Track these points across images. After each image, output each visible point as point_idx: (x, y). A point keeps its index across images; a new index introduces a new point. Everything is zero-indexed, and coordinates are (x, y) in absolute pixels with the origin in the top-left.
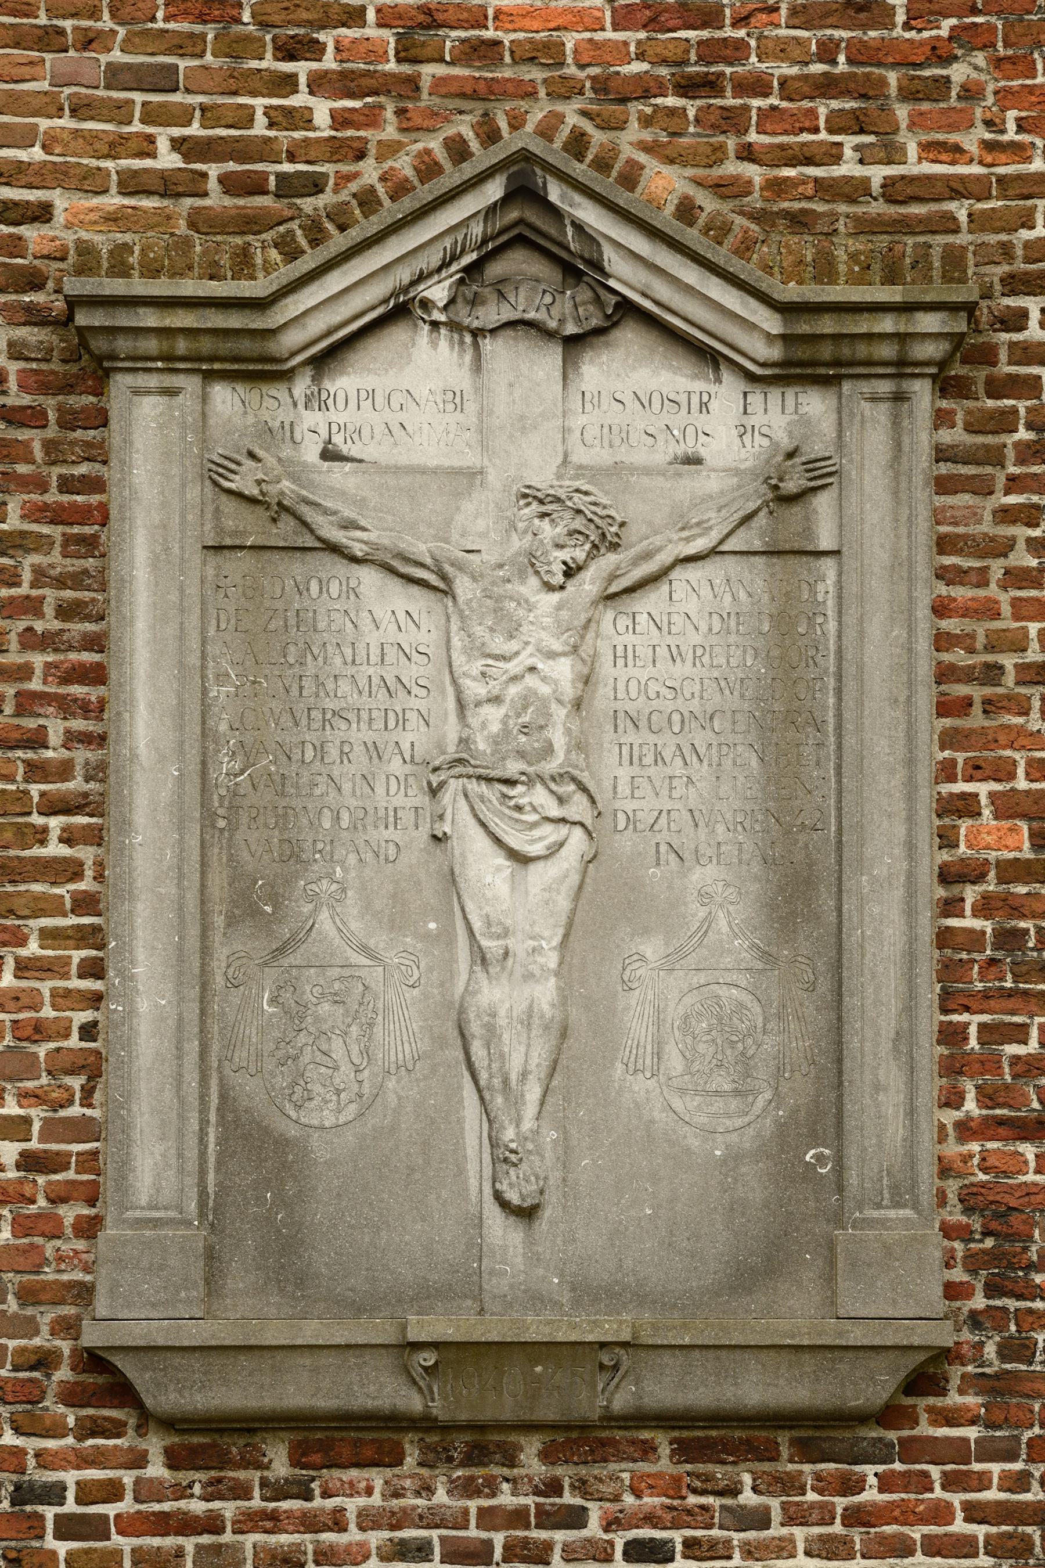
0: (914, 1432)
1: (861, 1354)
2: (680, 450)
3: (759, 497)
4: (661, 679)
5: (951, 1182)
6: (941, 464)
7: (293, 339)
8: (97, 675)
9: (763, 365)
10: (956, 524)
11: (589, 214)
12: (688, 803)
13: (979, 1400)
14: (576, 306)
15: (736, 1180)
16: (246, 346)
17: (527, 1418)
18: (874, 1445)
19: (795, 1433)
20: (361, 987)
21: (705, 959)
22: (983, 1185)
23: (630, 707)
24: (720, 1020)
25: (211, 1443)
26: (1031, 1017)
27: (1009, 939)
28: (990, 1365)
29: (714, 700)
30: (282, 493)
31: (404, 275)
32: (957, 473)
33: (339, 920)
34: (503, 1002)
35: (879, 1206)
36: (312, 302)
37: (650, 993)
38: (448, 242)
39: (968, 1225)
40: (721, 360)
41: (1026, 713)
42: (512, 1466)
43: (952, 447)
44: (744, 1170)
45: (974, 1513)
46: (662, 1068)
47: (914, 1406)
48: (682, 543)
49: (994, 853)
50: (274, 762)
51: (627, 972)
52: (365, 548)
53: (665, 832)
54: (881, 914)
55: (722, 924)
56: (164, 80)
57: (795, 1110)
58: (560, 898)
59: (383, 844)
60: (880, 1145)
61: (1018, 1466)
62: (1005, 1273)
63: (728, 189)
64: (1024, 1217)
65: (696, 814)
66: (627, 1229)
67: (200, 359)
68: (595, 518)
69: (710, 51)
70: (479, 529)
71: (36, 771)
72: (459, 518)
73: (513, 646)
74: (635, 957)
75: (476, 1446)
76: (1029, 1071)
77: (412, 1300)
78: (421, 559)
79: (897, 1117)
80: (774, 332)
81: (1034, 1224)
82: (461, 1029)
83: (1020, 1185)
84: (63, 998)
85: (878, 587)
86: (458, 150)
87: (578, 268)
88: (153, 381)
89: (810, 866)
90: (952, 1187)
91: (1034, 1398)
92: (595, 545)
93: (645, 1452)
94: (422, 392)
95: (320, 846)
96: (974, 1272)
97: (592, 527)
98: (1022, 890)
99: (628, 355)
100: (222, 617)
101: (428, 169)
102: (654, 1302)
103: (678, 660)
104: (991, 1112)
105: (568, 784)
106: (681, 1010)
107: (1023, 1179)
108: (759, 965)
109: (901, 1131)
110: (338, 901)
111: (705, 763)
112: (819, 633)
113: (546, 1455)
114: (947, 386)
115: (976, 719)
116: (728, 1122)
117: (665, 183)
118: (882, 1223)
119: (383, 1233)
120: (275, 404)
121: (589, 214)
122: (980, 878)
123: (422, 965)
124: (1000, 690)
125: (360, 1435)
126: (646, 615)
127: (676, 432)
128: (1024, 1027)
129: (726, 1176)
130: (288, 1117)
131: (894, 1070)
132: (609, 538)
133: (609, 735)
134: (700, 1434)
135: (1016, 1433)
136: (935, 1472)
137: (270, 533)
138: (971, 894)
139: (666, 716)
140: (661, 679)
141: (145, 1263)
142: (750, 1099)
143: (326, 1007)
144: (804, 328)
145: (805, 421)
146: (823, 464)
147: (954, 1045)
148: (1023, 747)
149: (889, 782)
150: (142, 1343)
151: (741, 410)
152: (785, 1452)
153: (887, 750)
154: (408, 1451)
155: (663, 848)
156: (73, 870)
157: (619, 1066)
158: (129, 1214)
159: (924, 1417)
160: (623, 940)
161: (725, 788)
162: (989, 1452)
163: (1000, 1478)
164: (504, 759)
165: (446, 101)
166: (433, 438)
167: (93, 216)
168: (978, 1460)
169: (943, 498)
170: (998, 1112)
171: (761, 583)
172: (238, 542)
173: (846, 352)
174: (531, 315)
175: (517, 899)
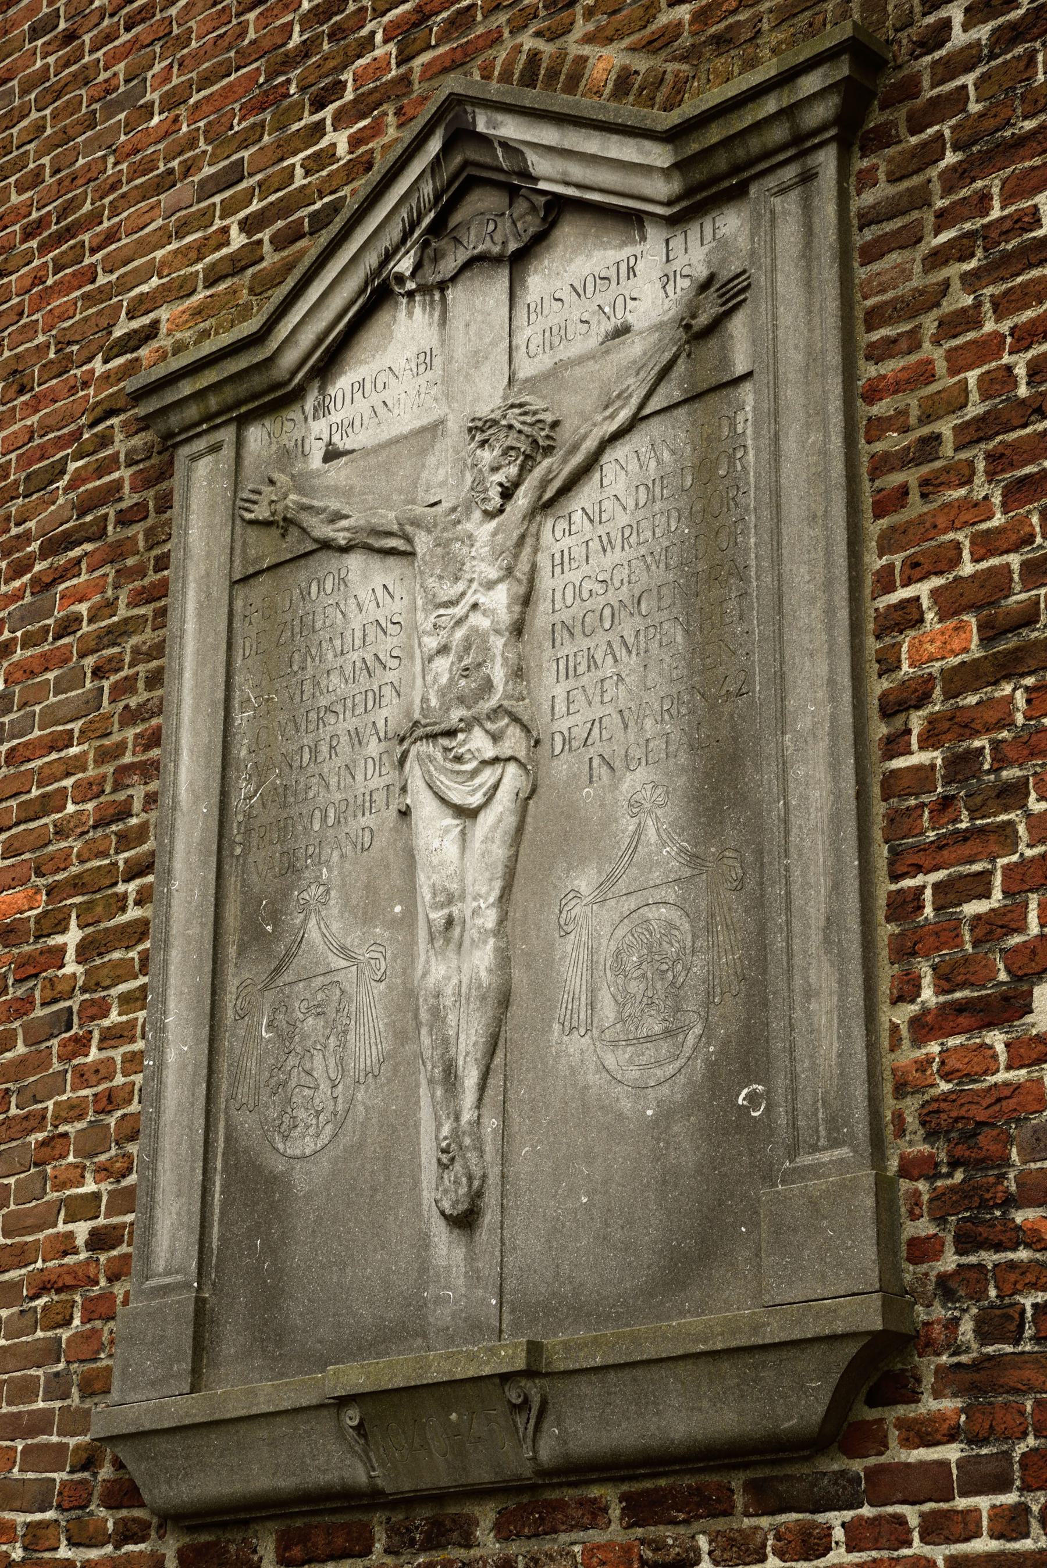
0: (882, 1459)
1: (784, 1354)
2: (609, 326)
3: (675, 344)
4: (593, 576)
5: (909, 1100)
6: (866, 230)
7: (291, 357)
9: (669, 204)
10: (884, 291)
11: (510, 129)
12: (611, 703)
13: (958, 1403)
14: (514, 223)
15: (668, 1143)
16: (257, 382)
17: (463, 1481)
18: (836, 1483)
19: (750, 1474)
20: (338, 992)
21: (635, 880)
22: (945, 1097)
23: (565, 616)
24: (650, 947)
26: (993, 860)
27: (961, 765)
28: (967, 1351)
29: (643, 579)
30: (287, 507)
31: (372, 259)
34: (449, 978)
35: (815, 1149)
36: (297, 319)
37: (584, 932)
38: (404, 213)
39: (931, 1156)
40: (644, 216)
41: (970, 481)
42: (468, 1546)
43: (873, 207)
44: (676, 1129)
46: (596, 1019)
47: (882, 1420)
48: (607, 422)
49: (938, 664)
50: (279, 776)
51: (564, 915)
52: (347, 535)
53: (598, 743)
54: (807, 775)
55: (651, 832)
57: (726, 1042)
58: (494, 846)
59: (360, 832)
60: (814, 1067)
61: (1011, 1498)
62: (978, 1217)
64: (995, 1132)
65: (626, 713)
66: (563, 1226)
67: (229, 409)
68: (525, 428)
72: (424, 475)
73: (460, 587)
74: (571, 896)
76: (991, 932)
77: (371, 1345)
78: (388, 528)
79: (831, 1026)
80: (666, 165)
81: (1010, 1140)
83: (990, 1088)
87: (516, 184)
88: (201, 444)
89: (735, 739)
90: (911, 1106)
91: (1024, 1393)
93: (594, 1516)
94: (400, 364)
95: (311, 850)
96: (940, 1220)
97: (523, 438)
98: (972, 700)
99: (565, 251)
100: (247, 644)
102: (589, 1315)
103: (609, 549)
104: (949, 997)
105: (503, 718)
106: (613, 948)
107: (992, 1079)
108: (687, 872)
109: (836, 1045)
110: (323, 904)
111: (634, 653)
112: (739, 468)
113: (503, 1531)
115: (916, 507)
116: (659, 1072)
118: (814, 1171)
119: (348, 1270)
121: (510, 129)
122: (923, 700)
123: (388, 955)
124: (938, 464)
125: (334, 1519)
126: (580, 512)
127: (607, 309)
128: (986, 876)
129: (658, 1140)
130: (277, 1150)
131: (826, 966)
132: (541, 443)
133: (548, 653)
134: (648, 1485)
135: (1005, 1447)
136: (912, 1514)
138: (917, 722)
139: (598, 614)
140: (593, 576)
141: (149, 1339)
142: (681, 1036)
143: (310, 1021)
144: (694, 147)
145: (723, 244)
146: (736, 282)
147: (905, 918)
148: (966, 524)
149: (809, 615)
150: (132, 1429)
151: (664, 259)
152: (739, 1500)
153: (807, 578)
154: (377, 1536)
155: (596, 762)
157: (556, 1027)
158: (149, 1284)
159: (894, 1434)
160: (560, 878)
161: (652, 676)
163: (990, 1519)
164: (448, 709)
165: (432, 82)
167: (185, 317)
168: (964, 1494)
169: (869, 268)
170: (958, 995)
171: (682, 435)
172: (257, 568)
173: (740, 153)
174: (481, 248)
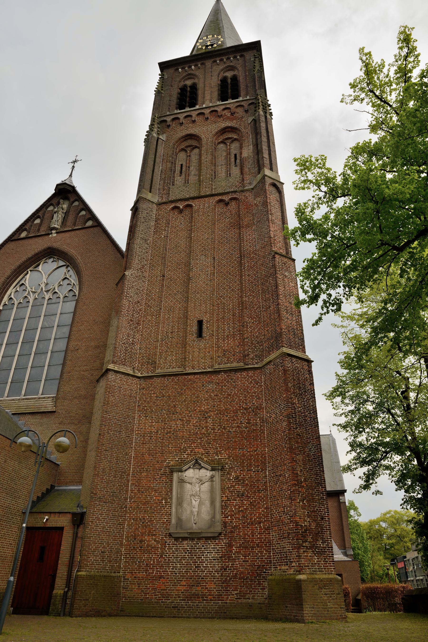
8: (172, 490)
11: (200, 462)
12: (206, 497)
25: (176, 539)
27: (226, 505)
32: (222, 476)
33: (185, 505)
45: (223, 543)
56: (177, 455)
63: (209, 459)
69: (208, 451)
70: (194, 480)
71: (168, 496)
75: (192, 539)
82: (192, 512)
84: (169, 510)
85: (217, 483)
86: (194, 458)
87: (200, 465)
92: (201, 482)
101: (192, 459)
114: (221, 470)
117: (205, 459)
120: (182, 473)
121: (200, 462)
137: (182, 481)
156: (170, 502)
162: (224, 539)
166: (191, 475)
175: (195, 503)
